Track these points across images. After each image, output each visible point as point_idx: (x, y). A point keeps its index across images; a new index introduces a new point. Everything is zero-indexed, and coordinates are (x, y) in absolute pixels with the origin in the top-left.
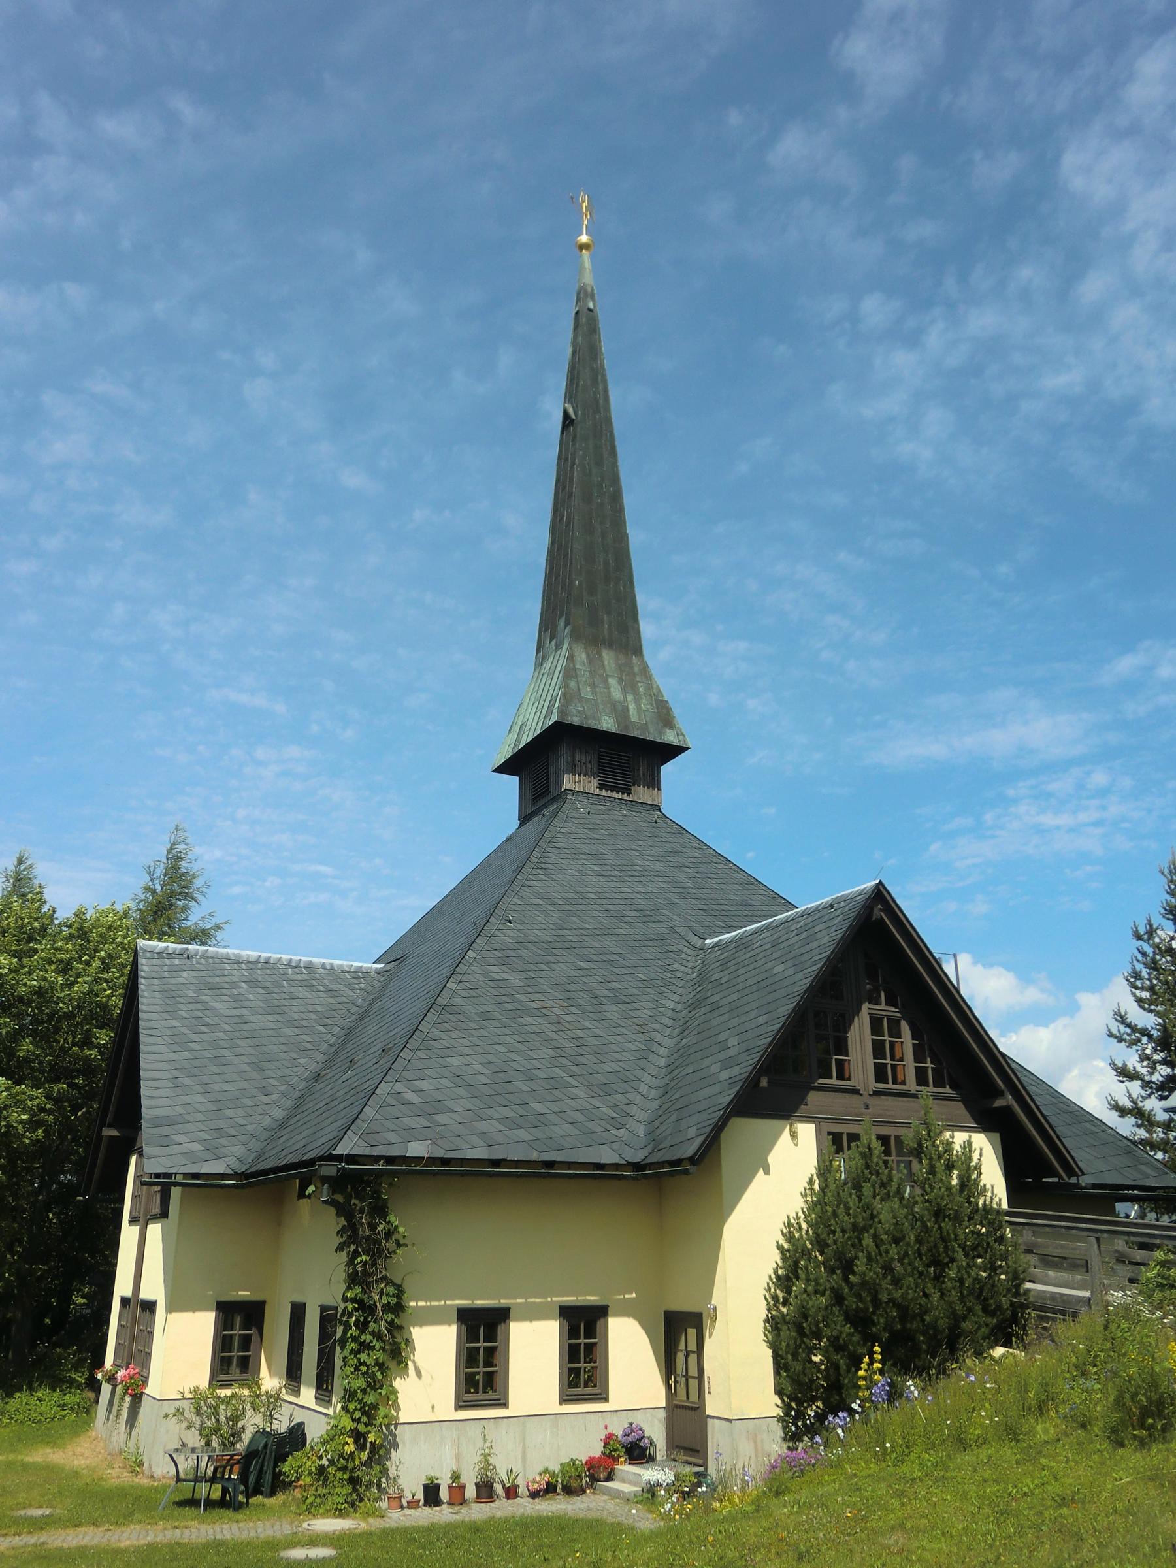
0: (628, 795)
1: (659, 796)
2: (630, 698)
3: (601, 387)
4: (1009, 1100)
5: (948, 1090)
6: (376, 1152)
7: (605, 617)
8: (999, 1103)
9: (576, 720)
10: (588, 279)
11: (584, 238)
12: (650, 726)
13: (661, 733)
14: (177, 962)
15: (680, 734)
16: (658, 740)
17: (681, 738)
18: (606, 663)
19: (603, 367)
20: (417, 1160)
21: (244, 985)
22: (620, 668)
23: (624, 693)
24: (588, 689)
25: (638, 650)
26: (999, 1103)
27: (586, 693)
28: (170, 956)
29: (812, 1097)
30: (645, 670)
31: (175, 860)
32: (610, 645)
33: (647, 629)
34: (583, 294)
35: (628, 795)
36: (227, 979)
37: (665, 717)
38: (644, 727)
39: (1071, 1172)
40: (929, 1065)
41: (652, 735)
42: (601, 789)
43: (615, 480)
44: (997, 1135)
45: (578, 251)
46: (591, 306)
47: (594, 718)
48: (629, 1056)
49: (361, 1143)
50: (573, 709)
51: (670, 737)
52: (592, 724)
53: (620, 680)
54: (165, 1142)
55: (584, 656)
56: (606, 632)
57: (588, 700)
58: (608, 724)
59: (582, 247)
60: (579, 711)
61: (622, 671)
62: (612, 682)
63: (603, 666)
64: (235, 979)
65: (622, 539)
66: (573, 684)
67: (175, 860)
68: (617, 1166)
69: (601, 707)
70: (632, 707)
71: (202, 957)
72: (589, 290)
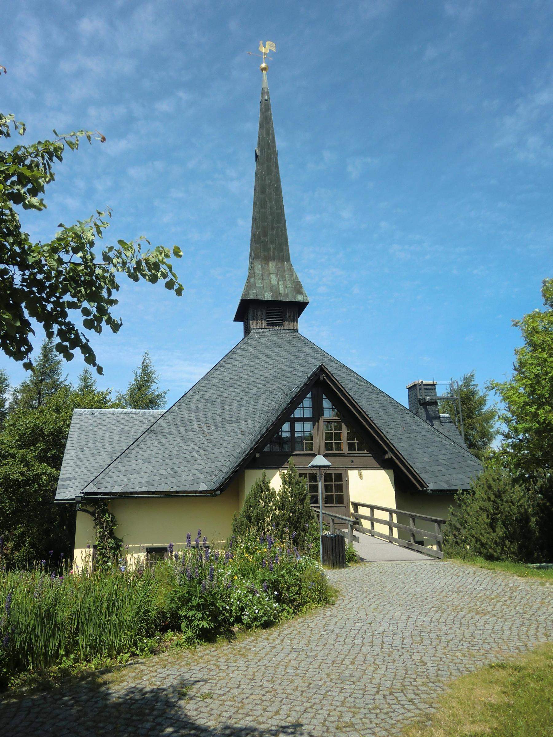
0: (281, 327)
1: (297, 325)
2: (281, 282)
3: (271, 137)
4: (390, 455)
5: (366, 452)
6: (99, 491)
7: (271, 246)
8: (386, 457)
9: (252, 297)
10: (265, 85)
11: (263, 65)
12: (289, 294)
13: (295, 297)
14: (88, 416)
15: (305, 296)
16: (293, 300)
17: (305, 298)
18: (271, 268)
19: (272, 127)
20: (116, 493)
21: (113, 423)
22: (277, 269)
23: (278, 280)
24: (260, 281)
25: (288, 259)
26: (386, 457)
27: (259, 283)
28: (86, 414)
29: (291, 459)
30: (291, 269)
31: (145, 366)
32: (274, 259)
33: (294, 249)
34: (264, 92)
35: (281, 327)
36: (107, 422)
37: (298, 288)
38: (287, 295)
39: (423, 486)
40: (356, 442)
41: (291, 299)
42: (268, 326)
43: (278, 180)
44: (392, 471)
45: (261, 71)
46: (266, 98)
47: (261, 295)
48: (231, 445)
49: (95, 487)
50: (251, 292)
51: (300, 298)
52: (260, 298)
53: (277, 275)
54: (65, 487)
55: (260, 266)
56: (271, 254)
57: (259, 287)
58: (268, 296)
59: (263, 69)
60: (254, 293)
61: (278, 270)
62: (273, 277)
63: (269, 270)
64: (110, 421)
65: (280, 207)
66: (252, 280)
67: (145, 366)
68: (206, 492)
69: (265, 289)
70: (281, 287)
71: (99, 413)
72: (266, 90)
